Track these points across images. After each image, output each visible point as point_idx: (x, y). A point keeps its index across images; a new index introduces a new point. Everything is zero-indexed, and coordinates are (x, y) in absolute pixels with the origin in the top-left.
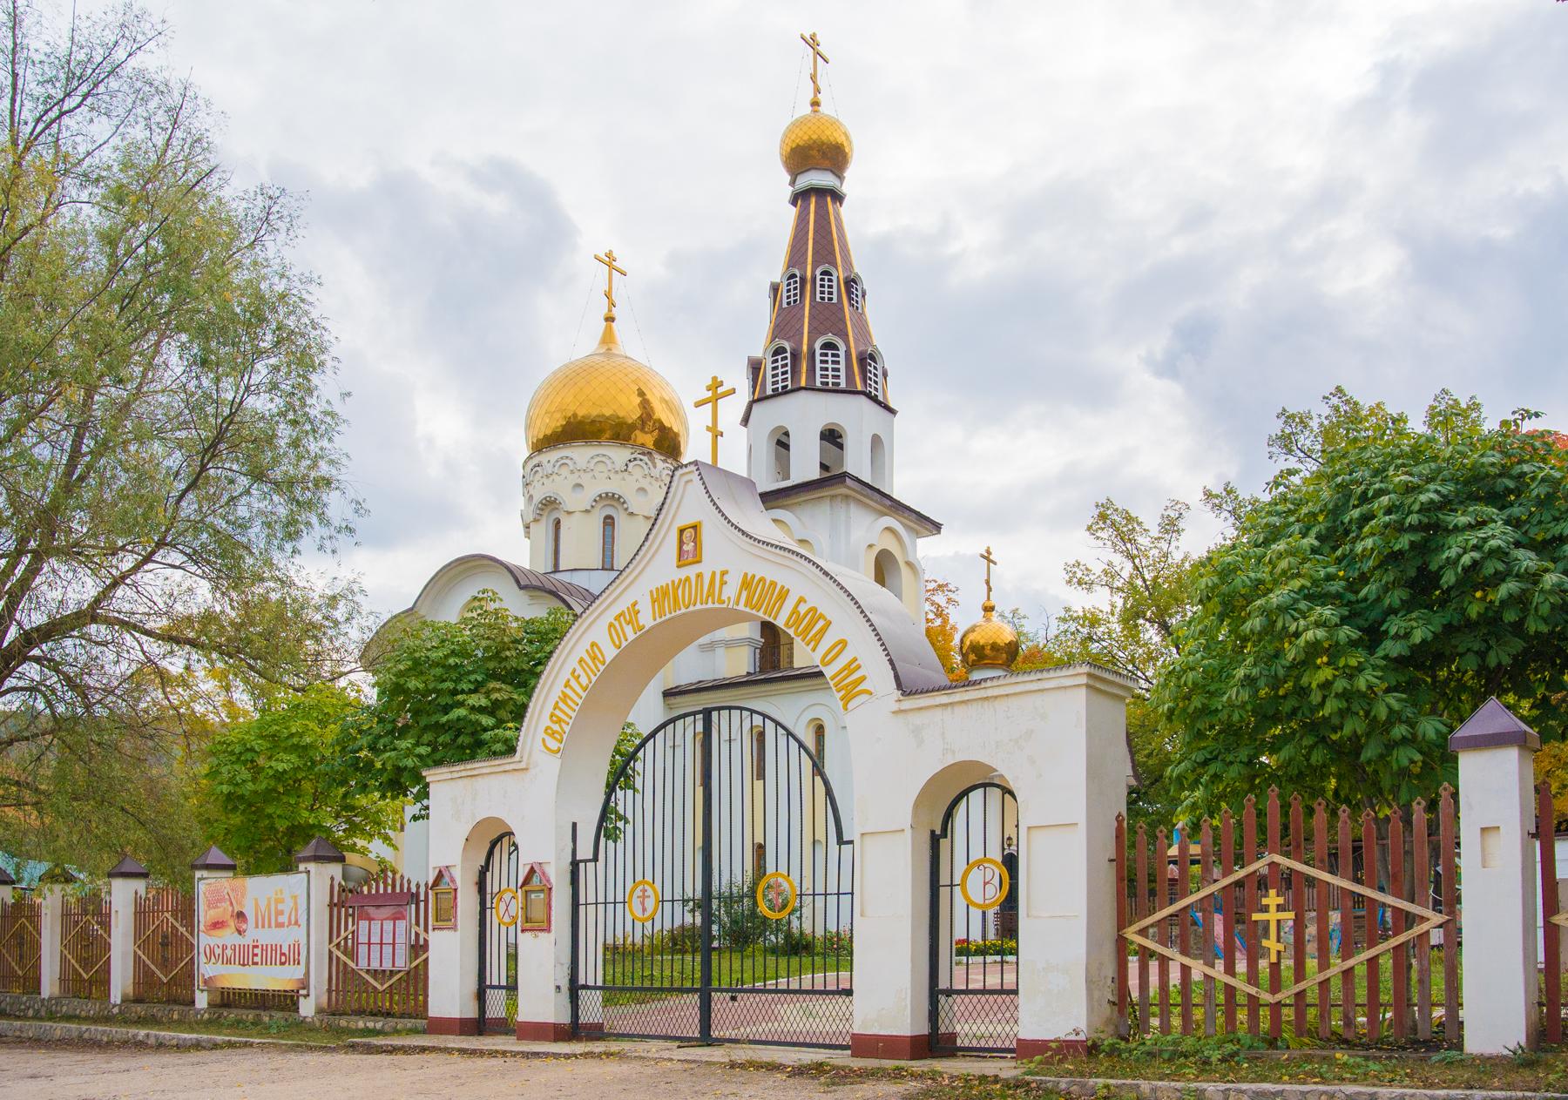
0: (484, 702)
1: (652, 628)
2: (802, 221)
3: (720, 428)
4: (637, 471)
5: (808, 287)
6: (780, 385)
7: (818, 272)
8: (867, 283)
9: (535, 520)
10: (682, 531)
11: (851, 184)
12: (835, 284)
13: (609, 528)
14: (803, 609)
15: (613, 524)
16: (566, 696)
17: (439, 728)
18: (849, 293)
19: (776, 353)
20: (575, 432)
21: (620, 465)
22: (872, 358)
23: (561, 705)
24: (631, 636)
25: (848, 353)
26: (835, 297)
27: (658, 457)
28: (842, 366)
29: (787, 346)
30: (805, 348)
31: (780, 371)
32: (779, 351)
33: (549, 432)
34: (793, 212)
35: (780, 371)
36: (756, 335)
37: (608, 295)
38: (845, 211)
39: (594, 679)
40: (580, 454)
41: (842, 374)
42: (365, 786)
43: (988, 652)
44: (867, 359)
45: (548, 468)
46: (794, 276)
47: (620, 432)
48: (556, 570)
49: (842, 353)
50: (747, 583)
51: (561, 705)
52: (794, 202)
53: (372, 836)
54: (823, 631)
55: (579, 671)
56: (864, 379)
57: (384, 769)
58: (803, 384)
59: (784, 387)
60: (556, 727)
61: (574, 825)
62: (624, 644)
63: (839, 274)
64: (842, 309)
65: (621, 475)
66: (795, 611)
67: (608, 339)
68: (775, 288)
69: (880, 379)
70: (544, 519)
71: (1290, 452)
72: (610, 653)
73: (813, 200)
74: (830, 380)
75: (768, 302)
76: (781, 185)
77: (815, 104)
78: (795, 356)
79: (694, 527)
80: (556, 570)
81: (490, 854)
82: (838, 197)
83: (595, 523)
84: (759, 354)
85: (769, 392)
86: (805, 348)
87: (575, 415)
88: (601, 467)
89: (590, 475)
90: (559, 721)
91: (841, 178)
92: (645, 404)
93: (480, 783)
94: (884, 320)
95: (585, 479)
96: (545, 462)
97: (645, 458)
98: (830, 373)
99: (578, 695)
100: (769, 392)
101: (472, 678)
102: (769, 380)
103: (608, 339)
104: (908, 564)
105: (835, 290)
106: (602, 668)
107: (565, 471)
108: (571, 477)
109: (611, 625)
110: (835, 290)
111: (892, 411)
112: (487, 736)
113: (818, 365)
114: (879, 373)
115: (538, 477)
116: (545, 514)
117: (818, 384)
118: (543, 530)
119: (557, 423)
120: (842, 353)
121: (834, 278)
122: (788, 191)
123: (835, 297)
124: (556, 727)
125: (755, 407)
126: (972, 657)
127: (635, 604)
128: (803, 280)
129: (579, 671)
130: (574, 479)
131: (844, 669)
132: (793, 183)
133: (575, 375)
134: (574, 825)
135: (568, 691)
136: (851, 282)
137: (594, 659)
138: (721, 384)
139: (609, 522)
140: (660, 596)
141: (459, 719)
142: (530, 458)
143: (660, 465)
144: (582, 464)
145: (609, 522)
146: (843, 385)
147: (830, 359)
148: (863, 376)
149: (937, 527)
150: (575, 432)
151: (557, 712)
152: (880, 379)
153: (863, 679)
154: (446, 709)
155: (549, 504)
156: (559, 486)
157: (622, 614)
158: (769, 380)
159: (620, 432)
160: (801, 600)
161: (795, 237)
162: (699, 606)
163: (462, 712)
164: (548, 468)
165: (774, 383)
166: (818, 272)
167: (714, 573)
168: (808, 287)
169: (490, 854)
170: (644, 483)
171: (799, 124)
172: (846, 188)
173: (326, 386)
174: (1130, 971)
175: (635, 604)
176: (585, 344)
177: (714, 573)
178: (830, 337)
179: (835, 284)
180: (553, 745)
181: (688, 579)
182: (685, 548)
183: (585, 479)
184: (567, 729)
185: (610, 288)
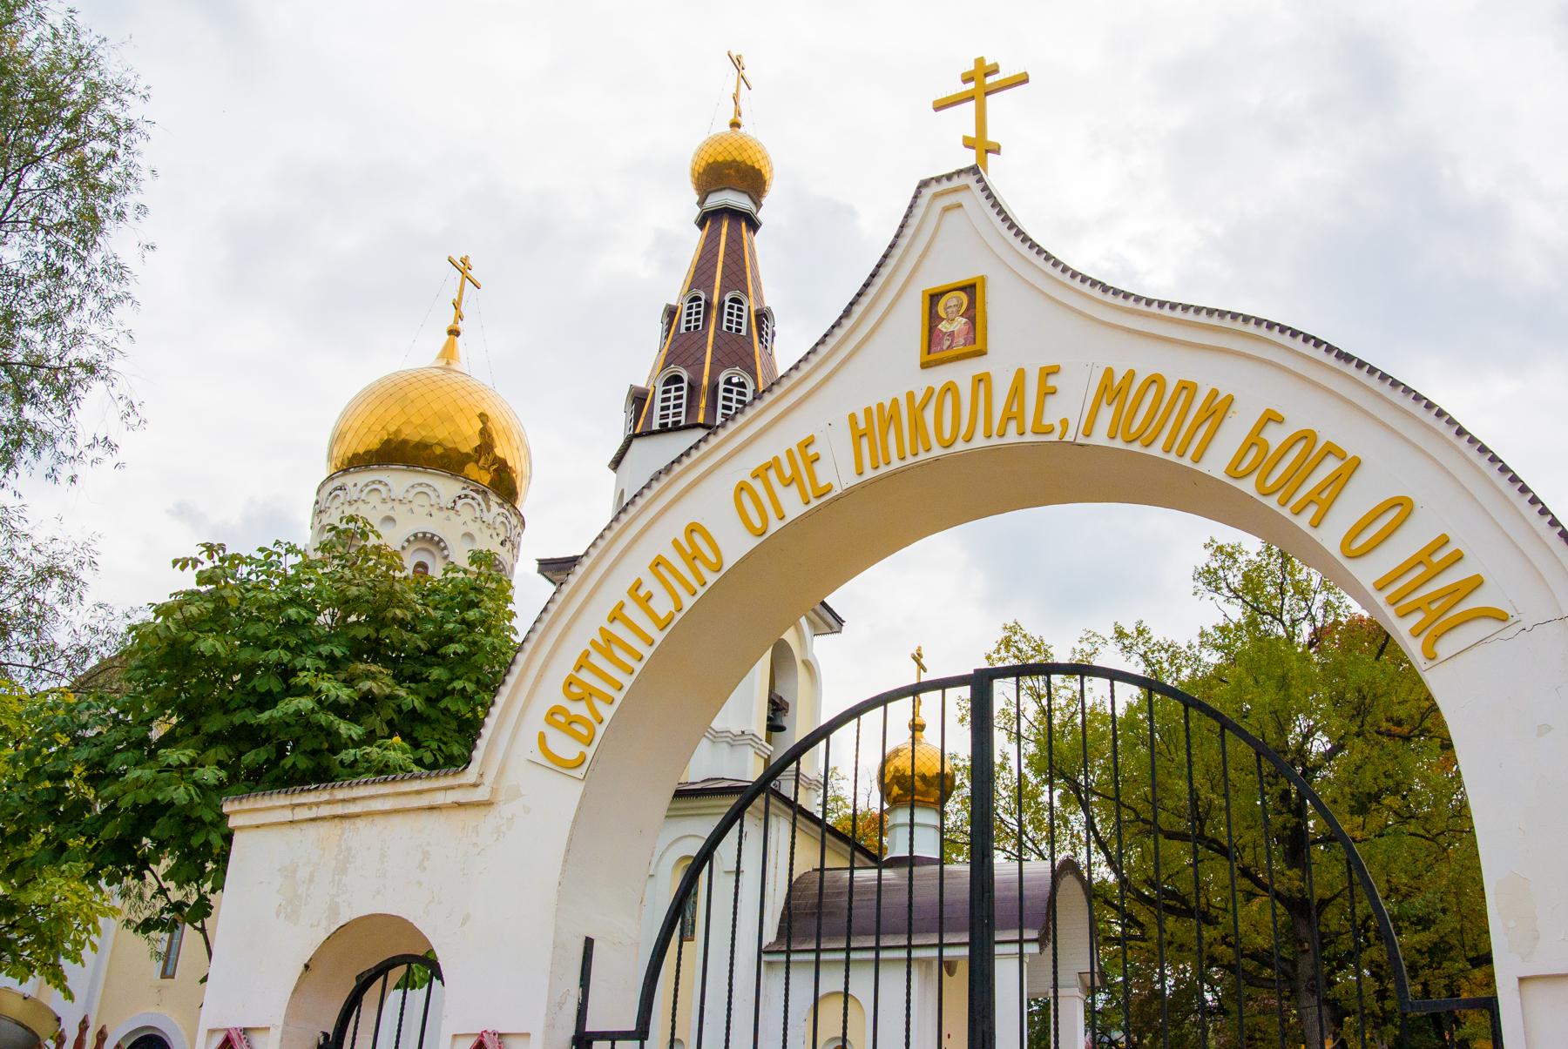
0: (344, 694)
1: (849, 492)
3: (992, 136)
4: (466, 513)
5: (714, 313)
6: (670, 420)
10: (934, 298)
12: (745, 315)
14: (1275, 437)
16: (610, 639)
17: (249, 736)
18: (760, 329)
20: (394, 453)
21: (446, 500)
23: (596, 659)
24: (794, 507)
26: (744, 329)
27: (494, 499)
29: (685, 375)
30: (705, 381)
31: (672, 403)
33: (361, 451)
34: (696, 237)
35: (672, 403)
36: (641, 359)
37: (456, 305)
39: (688, 602)
40: (398, 480)
42: (63, 847)
43: (918, 784)
45: (353, 493)
46: (697, 299)
47: (450, 463)
50: (1111, 390)
51: (596, 659)
53: (30, 968)
54: (1339, 481)
55: (651, 585)
57: (111, 811)
58: (701, 420)
59: (675, 423)
60: (579, 709)
61: (589, 943)
62: (775, 526)
63: (750, 305)
64: (751, 344)
65: (445, 513)
66: (1254, 440)
68: (671, 312)
71: (1217, 589)
72: (736, 544)
76: (687, 204)
77: (735, 125)
79: (970, 289)
81: (353, 1003)
82: (754, 225)
84: (642, 383)
85: (656, 427)
86: (705, 381)
87: (398, 431)
88: (422, 500)
89: (405, 508)
90: (588, 695)
91: (758, 205)
92: (485, 433)
93: (363, 835)
95: (400, 512)
96: (350, 485)
97: (479, 497)
99: (644, 637)
101: (325, 649)
102: (657, 413)
103: (448, 353)
104: (807, 664)
106: (712, 579)
107: (374, 499)
108: (381, 507)
109: (742, 488)
110: (744, 321)
112: (348, 755)
113: (720, 402)
115: (337, 502)
119: (373, 442)
121: (745, 308)
124: (579, 709)
125: (636, 444)
126: (896, 790)
127: (809, 443)
128: (708, 304)
129: (651, 585)
130: (385, 510)
131: (1417, 561)
132: (701, 203)
133: (394, 391)
134: (589, 943)
135: (618, 629)
136: (763, 316)
137: (693, 558)
138: (995, 70)
140: (869, 429)
141: (298, 713)
142: (331, 478)
143: (495, 509)
144: (398, 492)
150: (394, 453)
151: (585, 676)
153: (1476, 583)
154: (266, 701)
157: (774, 464)
158: (657, 413)
159: (450, 463)
160: (1271, 418)
161: (698, 268)
162: (979, 441)
163: (306, 703)
164: (353, 493)
165: (663, 417)
166: (727, 298)
167: (1021, 374)
168: (714, 313)
169: (353, 1003)
170: (473, 528)
171: (718, 140)
172: (761, 215)
173: (117, 241)
175: (809, 443)
176: (422, 352)
177: (1021, 374)
180: (567, 748)
181: (949, 388)
182: (944, 327)
183: (400, 512)
184: (608, 712)
185: (460, 298)
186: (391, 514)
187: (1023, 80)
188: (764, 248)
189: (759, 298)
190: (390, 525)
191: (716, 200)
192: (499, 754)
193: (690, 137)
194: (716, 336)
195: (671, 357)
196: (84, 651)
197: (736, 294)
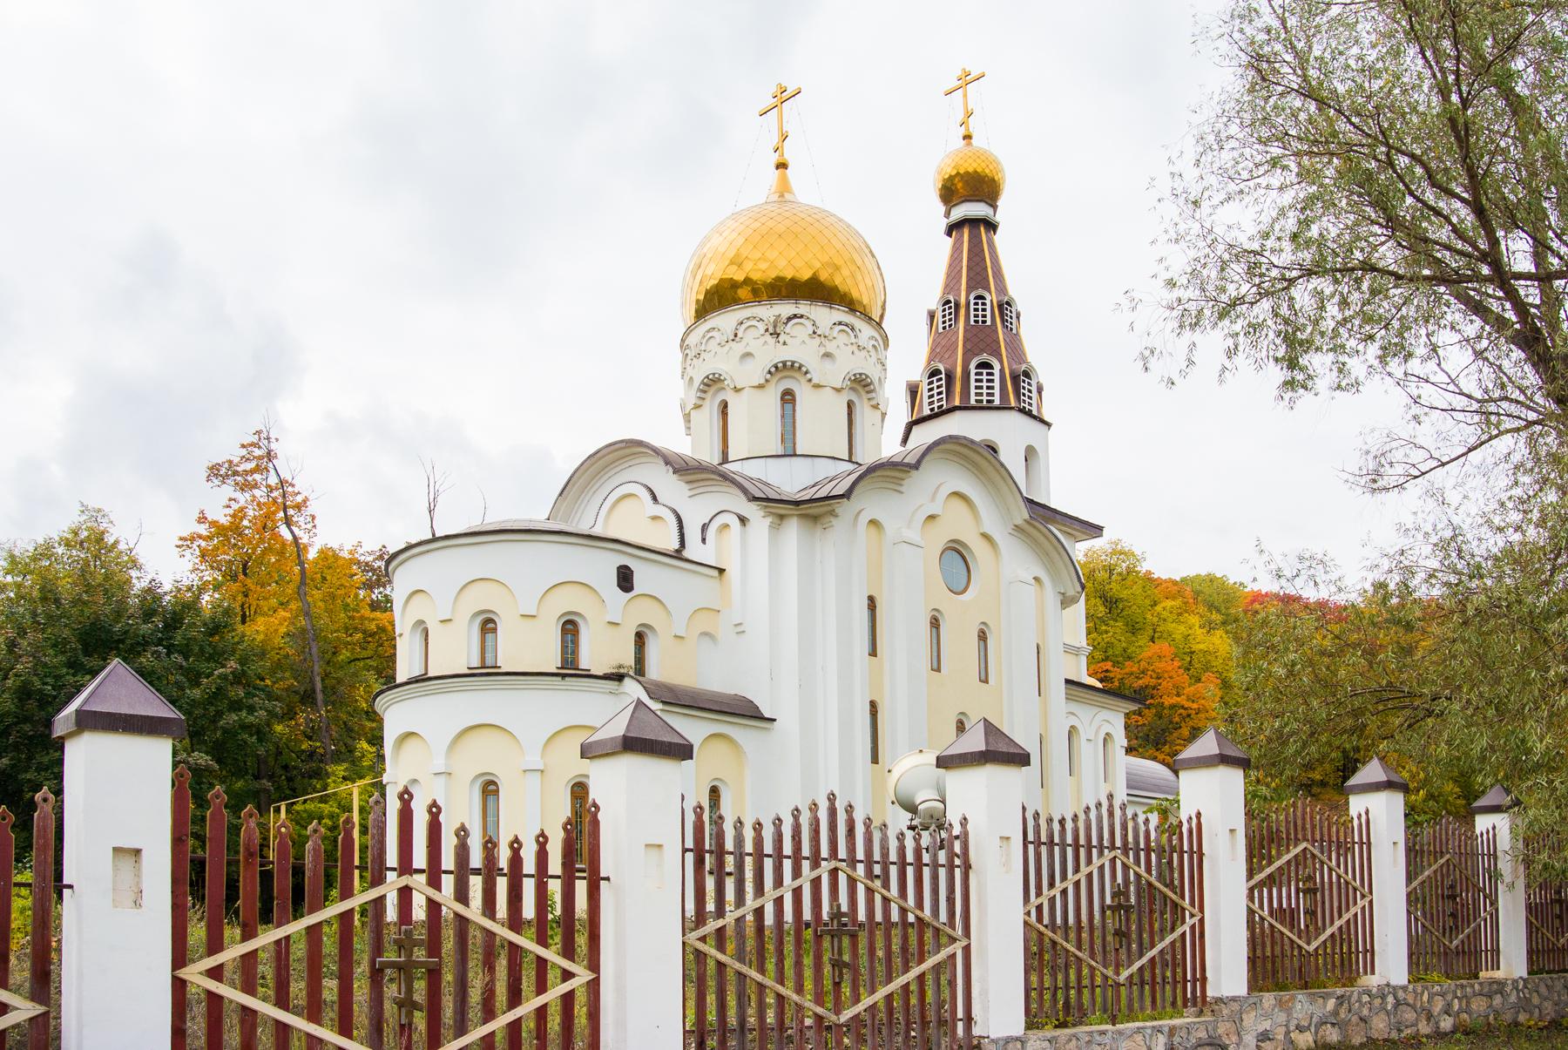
2: (957, 249)
7: (972, 297)
8: (1020, 305)
9: (697, 407)
11: (1004, 213)
12: (988, 307)
13: (788, 407)
15: (793, 401)
18: (1002, 315)
19: (932, 375)
22: (1027, 374)
25: (1002, 371)
26: (988, 319)
28: (997, 384)
30: (959, 370)
32: (934, 373)
38: (999, 238)
41: (997, 391)
44: (1020, 378)
46: (948, 302)
48: (725, 460)
49: (996, 371)
52: (949, 234)
56: (1018, 394)
58: (957, 403)
63: (991, 298)
67: (784, 189)
68: (932, 316)
69: (1034, 395)
70: (707, 403)
73: (966, 232)
74: (985, 398)
75: (926, 328)
78: (950, 378)
80: (725, 460)
82: (992, 226)
83: (771, 400)
84: (933, 307)
91: (995, 207)
94: (1040, 341)
98: (985, 384)
100: (927, 412)
105: (988, 313)
110: (988, 313)
111: (1048, 425)
114: (1034, 389)
116: (708, 396)
117: (973, 402)
118: (707, 418)
120: (996, 371)
122: (943, 224)
123: (988, 319)
125: (915, 429)
128: (957, 305)
132: (947, 215)
136: (1004, 306)
139: (788, 397)
145: (788, 397)
146: (997, 402)
147: (985, 377)
148: (1019, 393)
149: (1100, 529)
152: (1034, 395)
155: (712, 382)
156: (722, 362)
158: (926, 401)
165: (931, 403)
172: (999, 218)
174: (558, 1019)
178: (985, 357)
179: (988, 307)
186: (748, 350)
187: (714, 792)
188: (1007, 245)
189: (1002, 289)
190: (749, 359)
191: (959, 212)
192: (1042, 539)
193: (940, 155)
194: (966, 331)
195: (933, 355)
196: (1281, 738)
197: (980, 292)
